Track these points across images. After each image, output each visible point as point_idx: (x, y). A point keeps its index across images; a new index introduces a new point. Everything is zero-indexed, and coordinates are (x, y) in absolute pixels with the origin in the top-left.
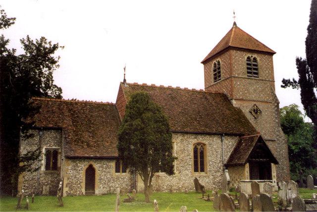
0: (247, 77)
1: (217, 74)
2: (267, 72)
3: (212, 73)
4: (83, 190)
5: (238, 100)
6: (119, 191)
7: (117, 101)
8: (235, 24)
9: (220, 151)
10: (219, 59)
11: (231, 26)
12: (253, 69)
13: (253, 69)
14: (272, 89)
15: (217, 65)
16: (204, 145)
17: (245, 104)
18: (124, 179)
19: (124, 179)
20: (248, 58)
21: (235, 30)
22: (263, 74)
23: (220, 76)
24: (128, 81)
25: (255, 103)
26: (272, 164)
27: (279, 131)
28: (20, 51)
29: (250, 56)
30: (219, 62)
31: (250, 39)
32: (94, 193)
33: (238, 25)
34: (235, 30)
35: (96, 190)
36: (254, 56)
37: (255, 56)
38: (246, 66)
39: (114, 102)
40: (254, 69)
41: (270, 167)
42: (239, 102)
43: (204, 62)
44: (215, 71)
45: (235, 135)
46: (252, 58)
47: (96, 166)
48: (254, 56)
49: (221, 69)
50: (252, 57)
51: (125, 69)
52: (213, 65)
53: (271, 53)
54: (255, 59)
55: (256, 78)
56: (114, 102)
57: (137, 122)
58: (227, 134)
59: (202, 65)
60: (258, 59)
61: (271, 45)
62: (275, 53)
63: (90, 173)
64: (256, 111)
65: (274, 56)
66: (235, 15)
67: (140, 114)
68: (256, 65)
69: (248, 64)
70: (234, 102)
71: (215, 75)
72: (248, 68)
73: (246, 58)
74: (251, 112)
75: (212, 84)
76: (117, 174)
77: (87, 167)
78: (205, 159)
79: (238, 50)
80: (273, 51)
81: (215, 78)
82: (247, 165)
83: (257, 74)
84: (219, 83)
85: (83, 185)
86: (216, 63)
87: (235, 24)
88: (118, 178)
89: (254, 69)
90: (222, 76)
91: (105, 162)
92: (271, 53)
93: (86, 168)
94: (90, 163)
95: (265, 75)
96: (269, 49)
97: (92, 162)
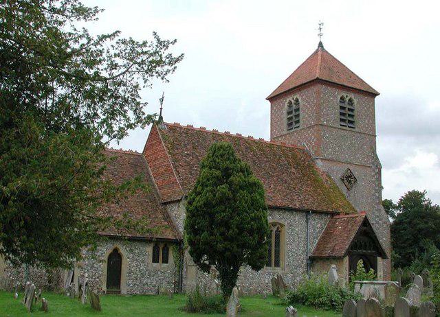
0: (340, 127)
1: (294, 118)
2: (367, 121)
3: (285, 117)
4: (104, 288)
5: (325, 160)
6: (411, 292)
7: (145, 149)
8: (321, 44)
9: (304, 236)
10: (297, 96)
13: (347, 117)
14: (372, 148)
15: (294, 106)
16: (282, 226)
17: (336, 167)
18: (164, 273)
19: (164, 273)
21: (321, 55)
22: (360, 123)
23: (297, 122)
24: (165, 120)
25: (349, 166)
26: (379, 259)
27: (379, 210)
30: (297, 100)
31: (351, 75)
32: (120, 292)
34: (321, 55)
35: (122, 287)
37: (351, 95)
38: (338, 110)
39: (140, 151)
40: (350, 115)
41: (376, 262)
42: (326, 163)
43: (271, 99)
44: (289, 113)
45: (327, 213)
46: (347, 99)
47: (123, 250)
49: (301, 112)
51: (162, 100)
52: (286, 104)
53: (373, 94)
54: (350, 100)
55: (352, 129)
56: (140, 151)
57: (224, 188)
58: (315, 212)
59: (268, 103)
60: (355, 101)
61: (373, 82)
62: (378, 94)
63: (115, 261)
64: (349, 179)
65: (377, 99)
66: (318, 32)
67: (227, 173)
70: (319, 163)
71: (290, 119)
72: (341, 114)
74: (343, 180)
75: (284, 133)
76: (155, 264)
77: (110, 251)
78: (281, 248)
79: (329, 85)
80: (375, 90)
81: (290, 125)
82: (347, 259)
83: (352, 122)
84: (296, 132)
85: (104, 279)
86: (293, 101)
87: (321, 44)
88: (156, 272)
89: (350, 115)
90: (301, 122)
91: (138, 245)
92: (373, 94)
93: (108, 255)
94: (113, 247)
95: (364, 126)
96: (372, 88)
97: (119, 245)
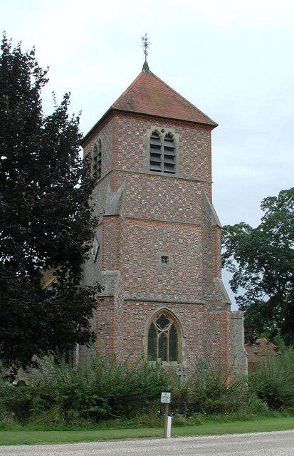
8: (146, 66)
11: (138, 70)
12: (162, 157)
13: (162, 157)
20: (155, 133)
21: (147, 82)
28: (48, 109)
29: (159, 129)
33: (152, 69)
34: (147, 82)
36: (167, 130)
46: (163, 135)
48: (167, 130)
50: (163, 131)
54: (169, 138)
56: (86, 117)
60: (177, 137)
62: (215, 126)
65: (213, 132)
68: (172, 149)
69: (153, 146)
73: (149, 134)
80: (206, 117)
87: (146, 66)
